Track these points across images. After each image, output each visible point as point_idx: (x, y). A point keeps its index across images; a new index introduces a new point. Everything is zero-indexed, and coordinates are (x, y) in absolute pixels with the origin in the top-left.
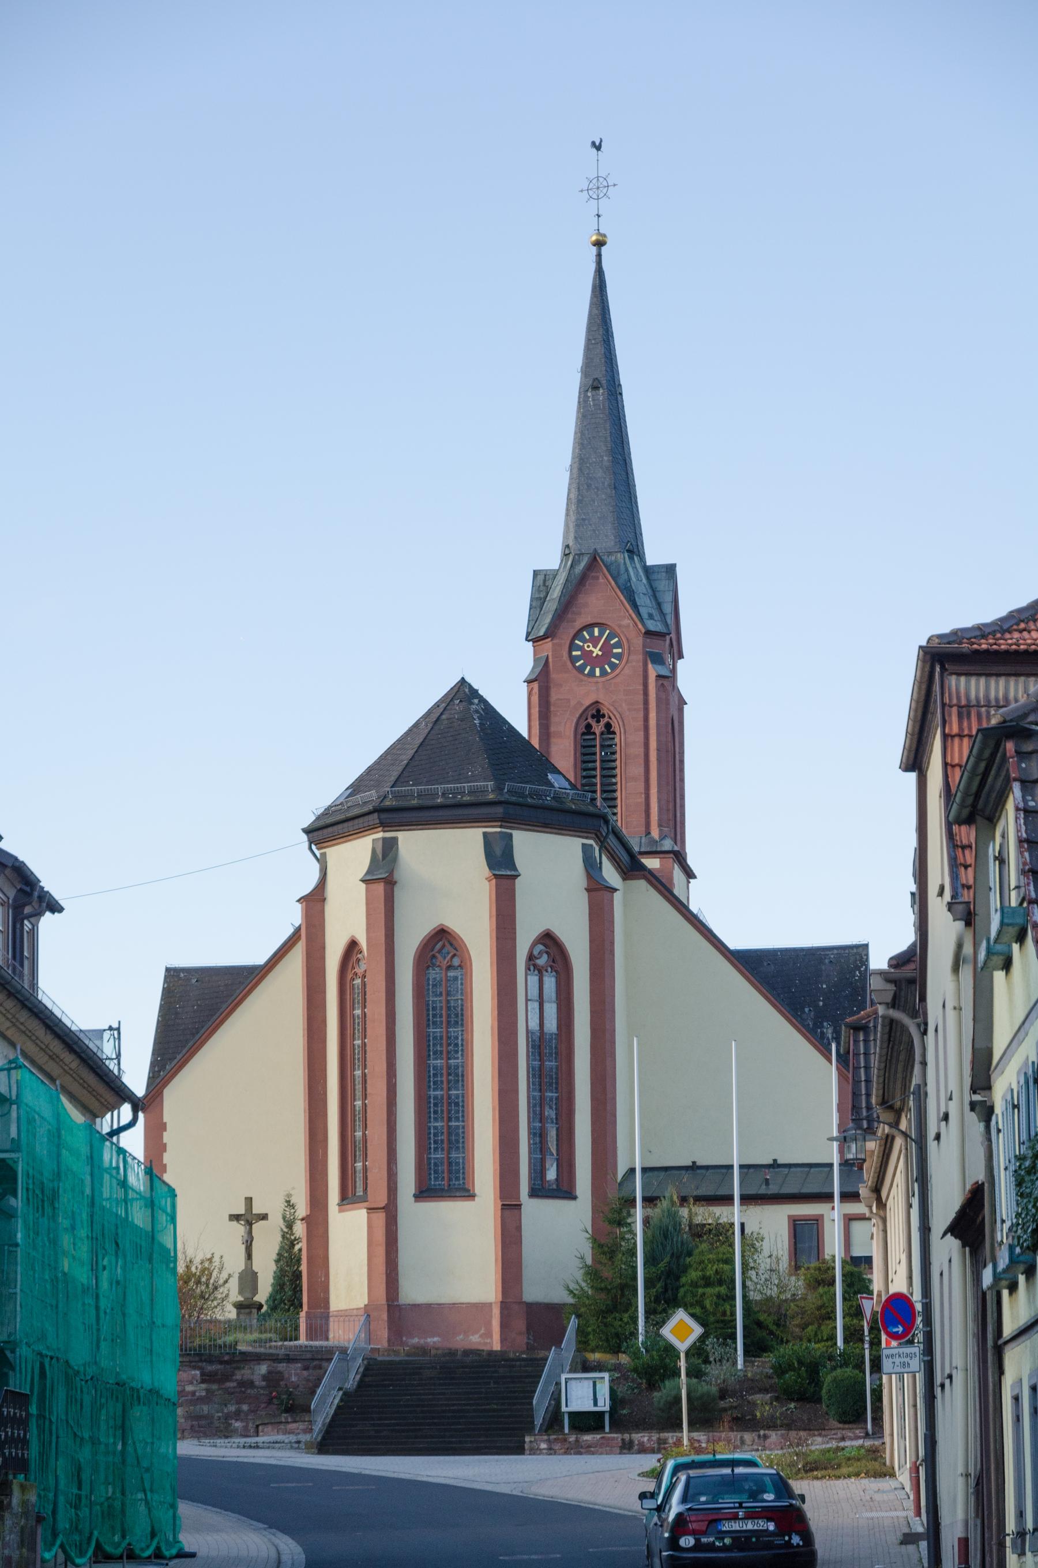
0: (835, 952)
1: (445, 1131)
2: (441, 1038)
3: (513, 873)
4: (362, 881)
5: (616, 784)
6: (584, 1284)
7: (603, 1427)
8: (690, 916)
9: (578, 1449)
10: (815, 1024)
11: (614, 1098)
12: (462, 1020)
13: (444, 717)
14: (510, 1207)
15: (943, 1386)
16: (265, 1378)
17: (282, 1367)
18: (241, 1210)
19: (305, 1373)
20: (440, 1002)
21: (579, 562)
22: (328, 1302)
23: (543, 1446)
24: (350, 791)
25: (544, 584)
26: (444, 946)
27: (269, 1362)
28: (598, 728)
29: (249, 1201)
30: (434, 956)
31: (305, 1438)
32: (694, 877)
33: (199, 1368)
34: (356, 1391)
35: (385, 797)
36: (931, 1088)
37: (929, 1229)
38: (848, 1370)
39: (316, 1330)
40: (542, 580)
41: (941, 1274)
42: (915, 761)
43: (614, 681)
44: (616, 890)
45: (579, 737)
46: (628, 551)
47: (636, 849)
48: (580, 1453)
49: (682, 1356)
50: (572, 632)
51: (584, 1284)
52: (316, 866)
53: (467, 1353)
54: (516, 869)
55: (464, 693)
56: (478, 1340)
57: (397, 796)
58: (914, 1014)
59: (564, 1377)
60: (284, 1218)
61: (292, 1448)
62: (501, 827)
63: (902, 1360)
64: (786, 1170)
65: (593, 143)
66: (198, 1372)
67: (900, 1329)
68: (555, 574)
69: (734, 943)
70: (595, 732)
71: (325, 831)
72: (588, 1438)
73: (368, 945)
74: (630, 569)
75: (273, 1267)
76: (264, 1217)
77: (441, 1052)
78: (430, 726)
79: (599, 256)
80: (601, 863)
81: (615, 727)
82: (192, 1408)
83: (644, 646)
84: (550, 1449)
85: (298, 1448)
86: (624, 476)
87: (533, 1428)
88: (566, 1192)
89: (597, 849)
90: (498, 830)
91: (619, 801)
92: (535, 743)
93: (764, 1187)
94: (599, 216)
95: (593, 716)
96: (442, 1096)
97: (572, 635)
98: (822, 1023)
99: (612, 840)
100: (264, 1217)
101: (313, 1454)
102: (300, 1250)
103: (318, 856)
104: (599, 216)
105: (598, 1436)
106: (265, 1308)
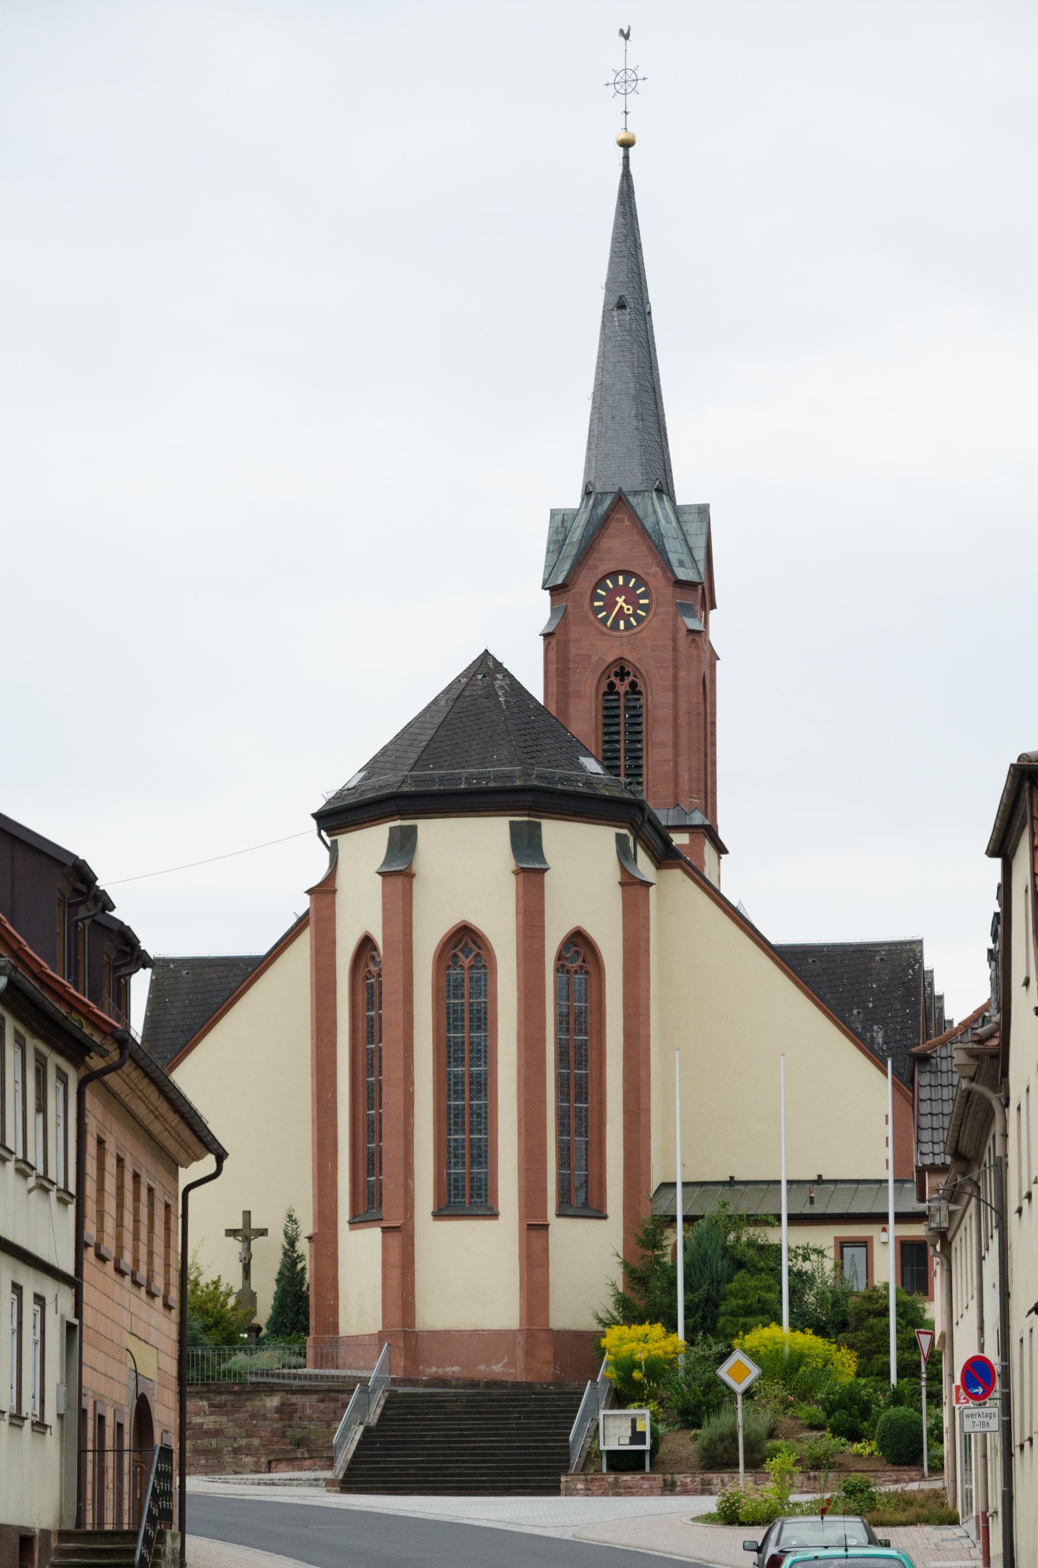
0: (887, 948)
1: (467, 1144)
2: (463, 1043)
3: (542, 866)
4: (380, 873)
5: (641, 750)
6: (615, 1313)
7: (643, 1468)
8: (729, 909)
9: (616, 1490)
10: (864, 1028)
11: (648, 1110)
12: (486, 1024)
13: (467, 693)
14: (534, 1229)
15: (1022, 1447)
16: (278, 1410)
17: (294, 1399)
18: (239, 1225)
19: (322, 1406)
20: (462, 1004)
21: (602, 501)
22: (338, 1327)
23: (580, 1486)
24: (363, 774)
25: (563, 526)
26: (466, 944)
27: (282, 1394)
28: (622, 688)
29: (247, 1215)
30: (455, 956)
31: (328, 1474)
32: (726, 852)
33: (208, 1399)
34: (377, 1425)
35: (403, 782)
36: (1012, 1160)
37: (1009, 1295)
38: (902, 1408)
39: (322, 1357)
40: (561, 521)
41: (1021, 1340)
42: (1002, 847)
43: (639, 635)
44: (651, 884)
45: (600, 697)
46: (657, 490)
47: (664, 823)
48: (619, 1494)
49: (739, 1398)
50: (594, 580)
51: (615, 1313)
52: (326, 854)
53: (491, 1384)
54: (545, 862)
55: (486, 666)
56: (500, 1370)
57: (417, 780)
58: (995, 1090)
59: (602, 1413)
60: (286, 1233)
61: (311, 1485)
62: (529, 815)
63: (982, 1419)
64: (832, 1187)
65: (621, 31)
66: (205, 1403)
67: (980, 1390)
68: (575, 514)
69: (776, 937)
70: (622, 696)
71: (337, 818)
72: (627, 1478)
73: (384, 943)
74: (659, 511)
75: (273, 1287)
76: (263, 1232)
77: (463, 1059)
78: (451, 703)
79: (626, 158)
80: (635, 854)
81: (641, 687)
82: (199, 1441)
83: (674, 597)
84: (588, 1489)
85: (317, 1486)
86: (653, 406)
87: (568, 1467)
88: (597, 1211)
89: (631, 839)
90: (526, 819)
91: (644, 769)
92: (552, 709)
93: (808, 1205)
94: (626, 113)
95: (616, 674)
96: (463, 1106)
97: (593, 583)
98: (871, 1026)
99: (648, 830)
100: (263, 1232)
101: (336, 1492)
102: (303, 1269)
103: (329, 844)
104: (626, 113)
105: (639, 1477)
106: (264, 1332)
